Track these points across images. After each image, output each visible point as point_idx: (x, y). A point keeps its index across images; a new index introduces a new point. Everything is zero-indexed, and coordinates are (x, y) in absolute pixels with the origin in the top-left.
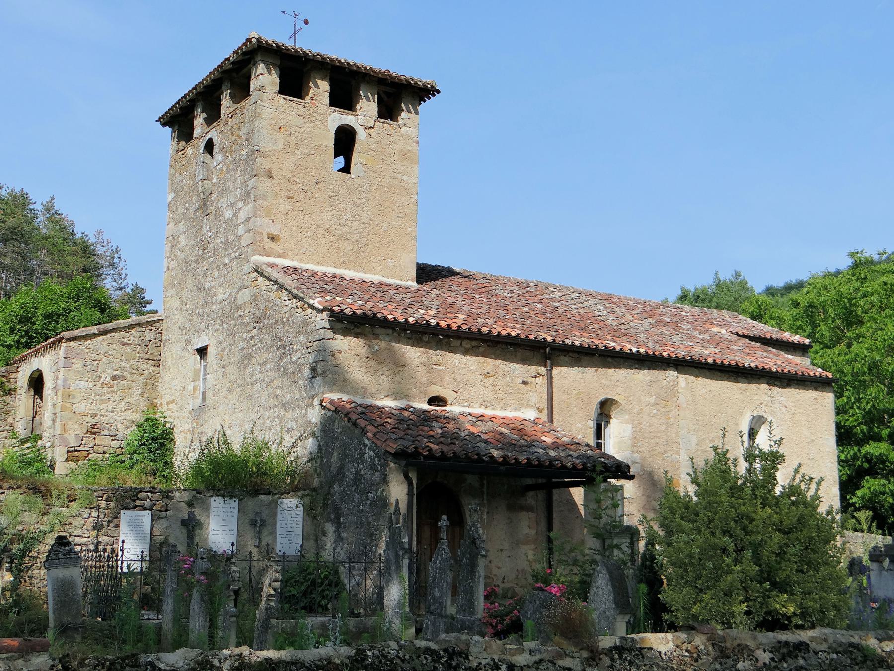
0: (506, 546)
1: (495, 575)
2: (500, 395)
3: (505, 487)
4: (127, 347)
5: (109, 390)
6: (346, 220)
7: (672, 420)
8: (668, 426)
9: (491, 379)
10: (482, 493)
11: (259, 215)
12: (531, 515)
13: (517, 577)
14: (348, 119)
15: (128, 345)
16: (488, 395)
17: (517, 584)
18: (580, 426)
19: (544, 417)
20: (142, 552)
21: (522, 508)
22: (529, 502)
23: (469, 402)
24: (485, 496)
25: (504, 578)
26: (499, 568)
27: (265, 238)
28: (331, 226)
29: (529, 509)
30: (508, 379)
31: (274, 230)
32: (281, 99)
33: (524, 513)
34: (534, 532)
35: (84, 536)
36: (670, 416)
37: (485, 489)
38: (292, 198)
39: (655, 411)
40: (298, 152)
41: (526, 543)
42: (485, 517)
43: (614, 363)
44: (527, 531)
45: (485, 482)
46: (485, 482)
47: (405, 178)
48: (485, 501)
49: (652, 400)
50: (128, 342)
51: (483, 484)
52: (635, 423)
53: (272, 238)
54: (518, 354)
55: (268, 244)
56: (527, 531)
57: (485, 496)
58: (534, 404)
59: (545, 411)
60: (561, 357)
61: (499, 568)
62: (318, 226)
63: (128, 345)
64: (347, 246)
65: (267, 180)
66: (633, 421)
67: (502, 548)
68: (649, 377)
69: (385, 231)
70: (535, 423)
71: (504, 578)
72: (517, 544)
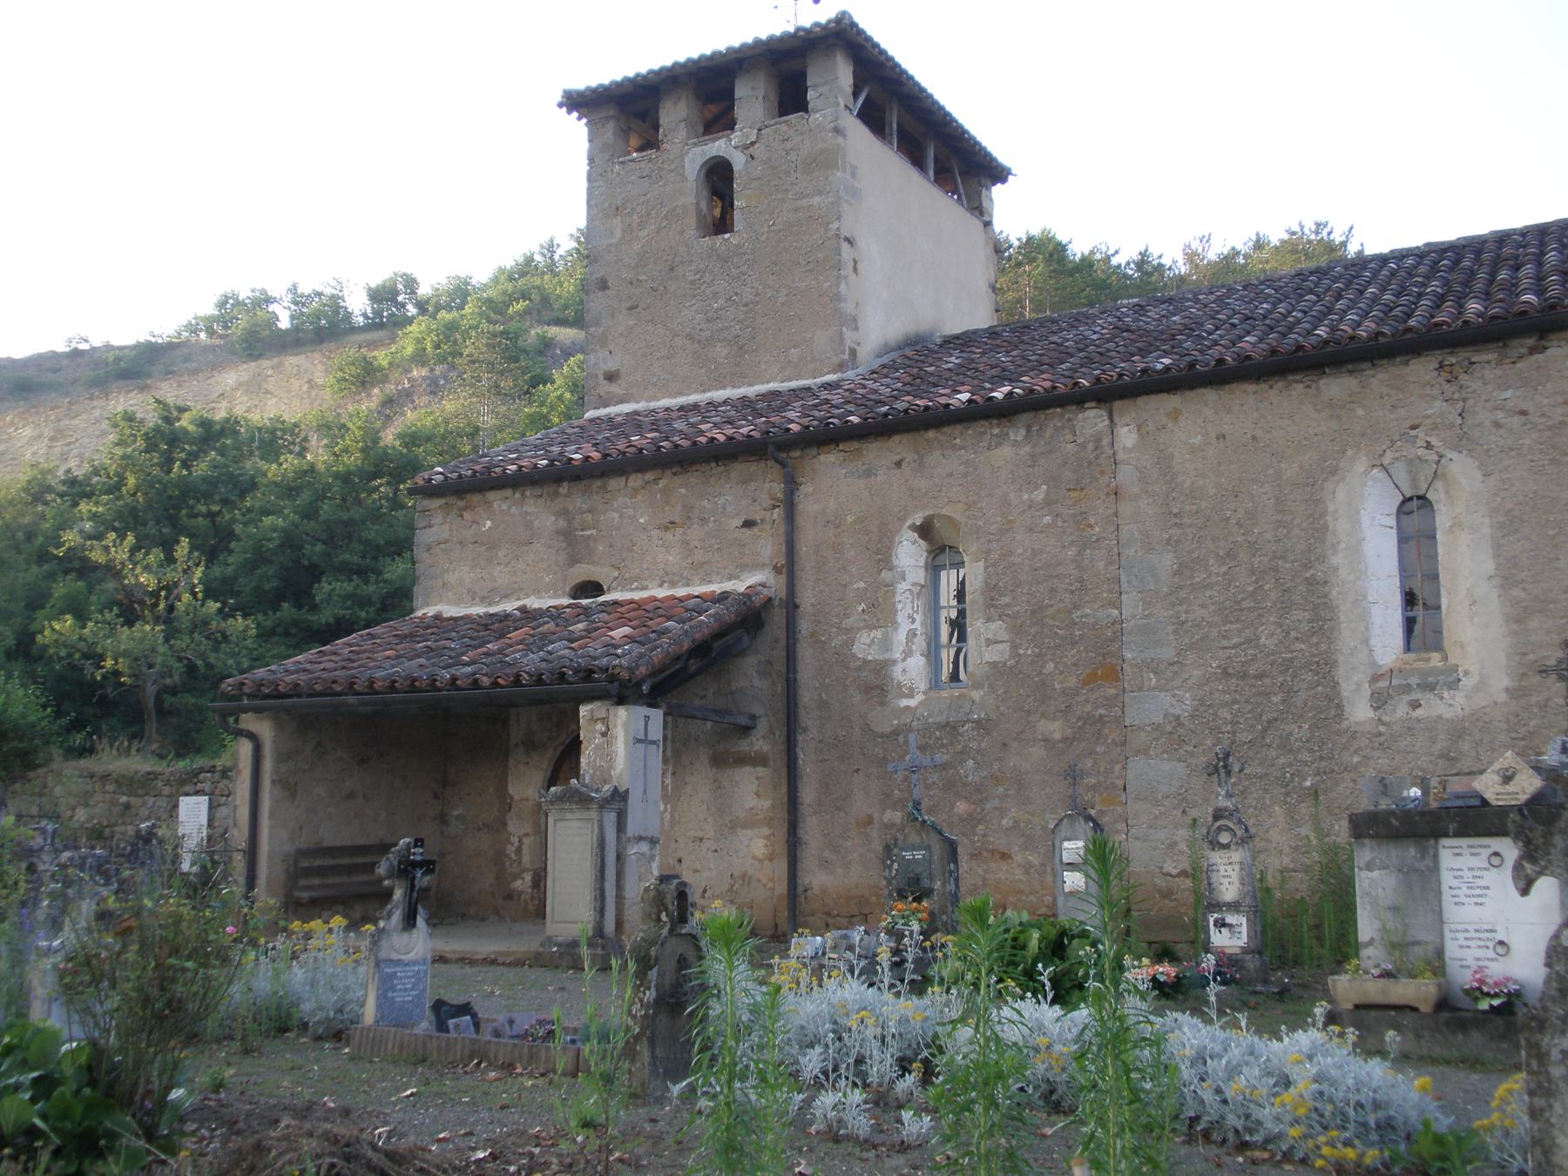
0: (709, 830)
2: (699, 556)
6: (717, 311)
7: (1097, 529)
8: (1085, 547)
9: (679, 531)
11: (592, 350)
12: (761, 771)
13: (731, 889)
16: (672, 558)
18: (862, 585)
20: (1141, 884)
21: (743, 760)
22: (756, 748)
23: (639, 581)
25: (705, 891)
26: (696, 871)
27: (601, 377)
28: (694, 328)
29: (759, 760)
30: (711, 525)
31: (611, 365)
33: (748, 769)
34: (767, 804)
36: (1092, 521)
38: (637, 307)
39: (1047, 519)
40: (641, 234)
41: (749, 824)
43: (942, 438)
44: (751, 802)
47: (816, 200)
49: (1040, 495)
52: (994, 556)
53: (611, 377)
54: (733, 474)
55: (606, 388)
56: (751, 802)
58: (767, 561)
60: (822, 458)
61: (696, 871)
62: (675, 336)
64: (721, 350)
65: (600, 294)
66: (988, 552)
67: (701, 834)
68: (1027, 448)
69: (783, 304)
71: (705, 891)
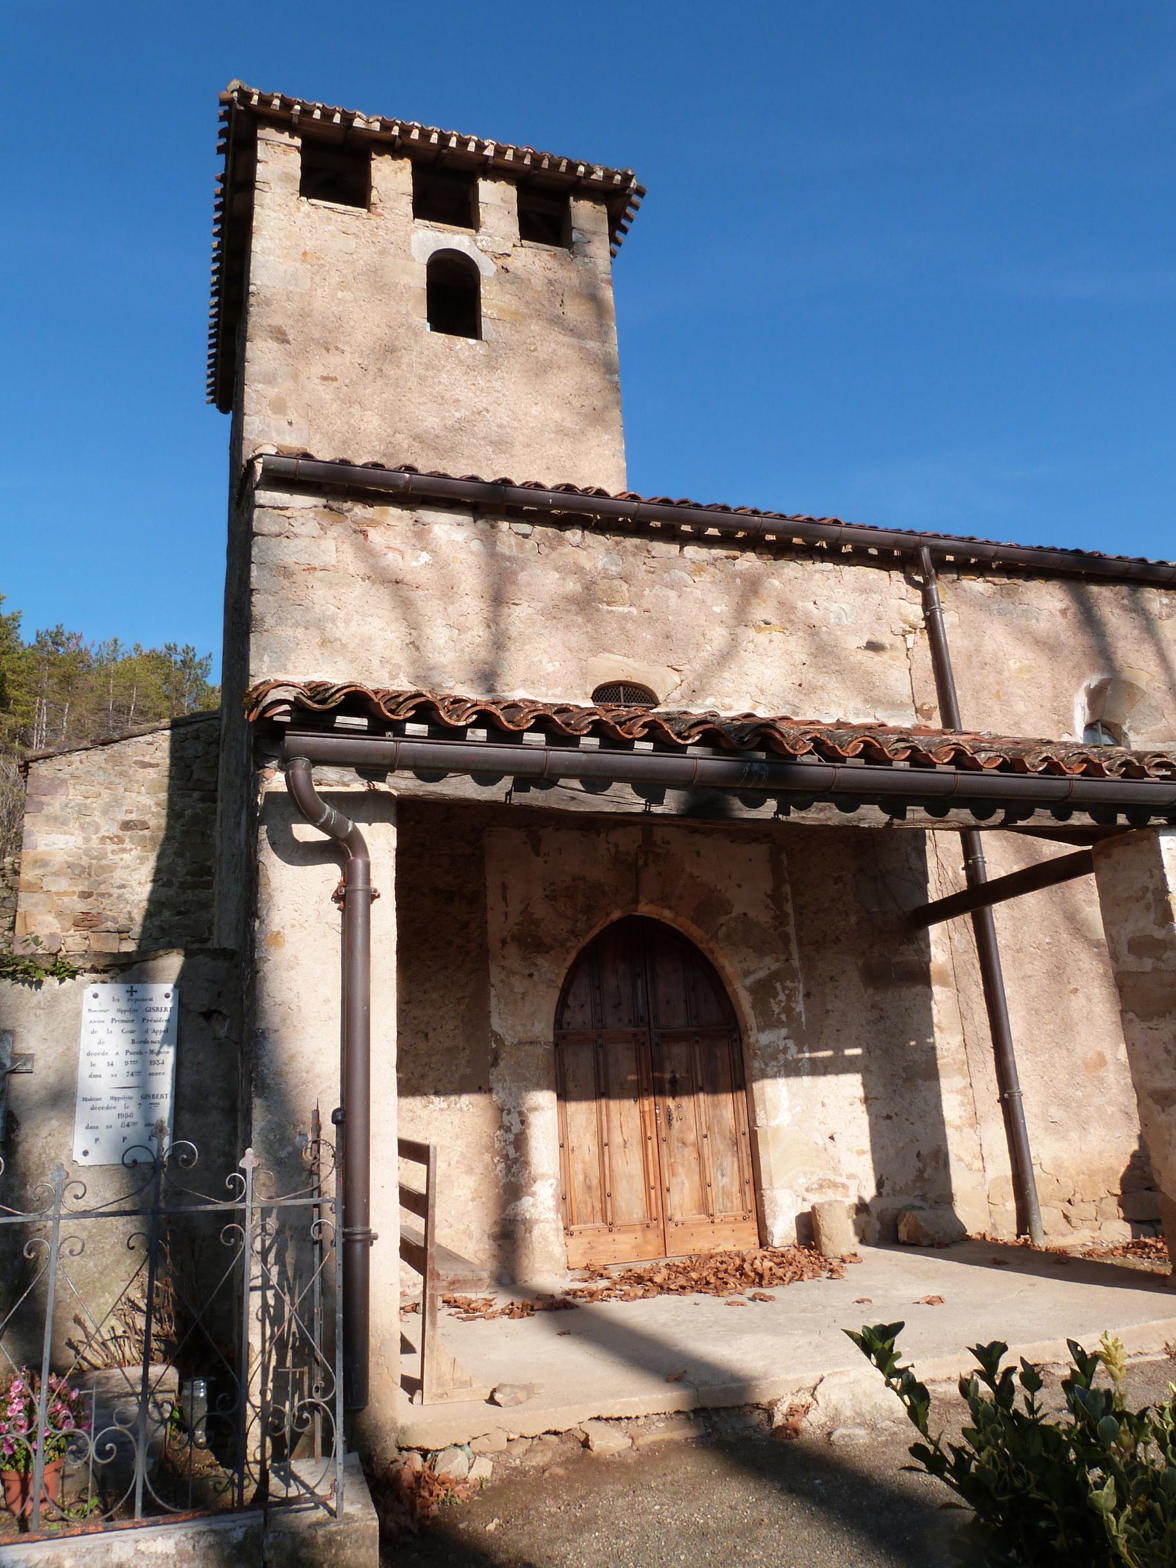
1: (851, 1176)
3: (853, 919)
4: (151, 770)
5: (115, 847)
10: (786, 939)
14: (456, 239)
15: (152, 766)
17: (923, 1197)
19: (936, 723)
24: (794, 947)
32: (306, 205)
35: (1151, 1352)
37: (791, 930)
38: (335, 379)
42: (800, 1007)
45: (789, 908)
46: (789, 908)
48: (796, 963)
50: (153, 761)
51: (787, 914)
57: (794, 947)
59: (937, 715)
63: (152, 766)
70: (783, 568)
72: (908, 1080)
